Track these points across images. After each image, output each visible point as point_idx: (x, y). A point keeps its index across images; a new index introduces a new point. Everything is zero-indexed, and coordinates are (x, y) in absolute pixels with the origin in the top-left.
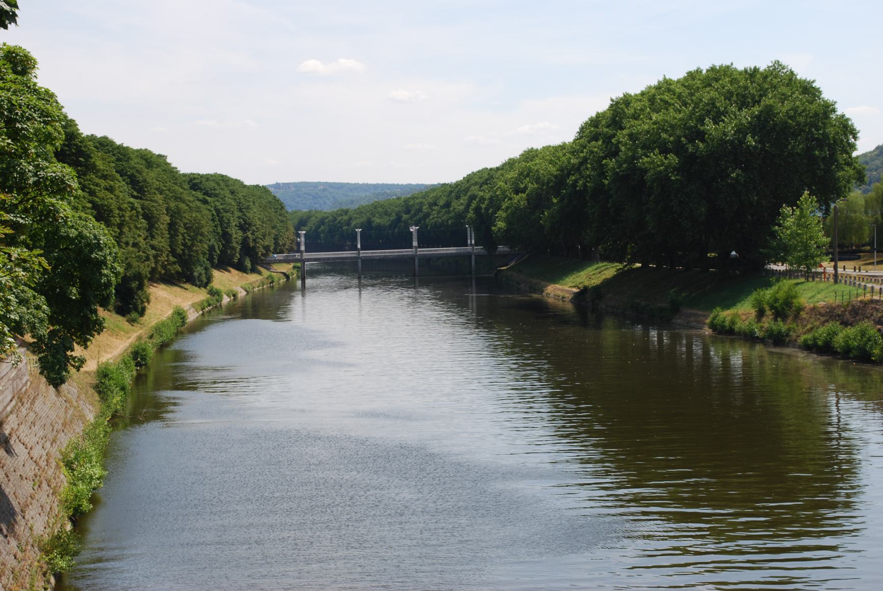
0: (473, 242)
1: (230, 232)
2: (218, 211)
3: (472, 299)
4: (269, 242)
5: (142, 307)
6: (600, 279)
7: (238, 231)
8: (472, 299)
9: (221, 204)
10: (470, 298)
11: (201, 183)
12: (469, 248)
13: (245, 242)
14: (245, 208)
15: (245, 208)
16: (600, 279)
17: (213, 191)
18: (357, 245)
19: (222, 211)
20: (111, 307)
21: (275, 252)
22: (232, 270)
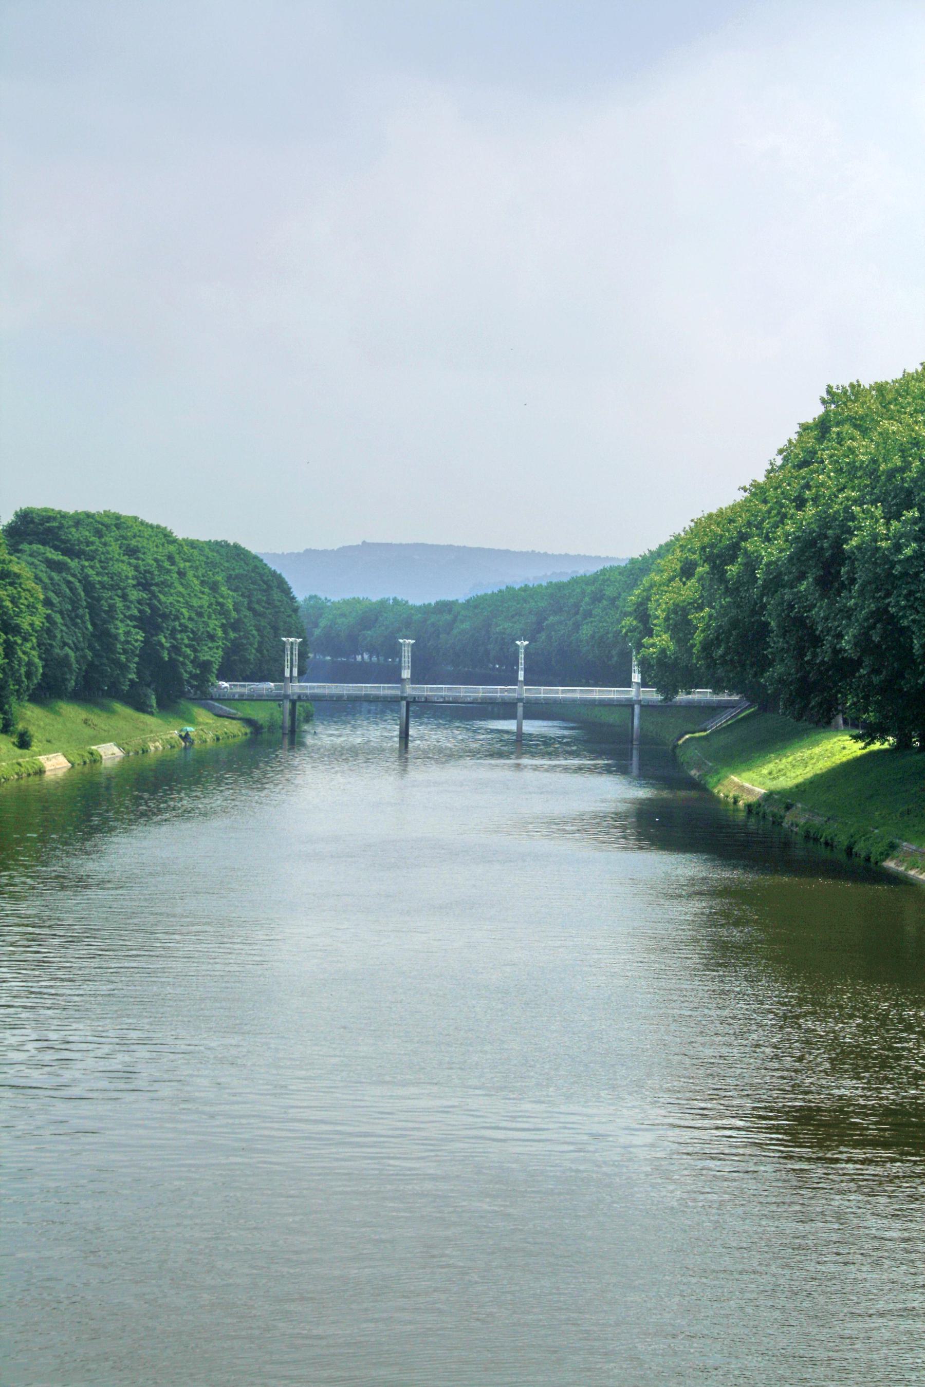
0: (295, 673)
1: (113, 631)
2: (89, 586)
3: (292, 648)
4: (213, 654)
5: (276, 690)
6: (824, 748)
7: (133, 631)
8: (292, 648)
9: (98, 574)
10: (288, 647)
11: (61, 527)
12: (632, 693)
13: (149, 653)
14: (157, 585)
15: (157, 585)
16: (824, 748)
17: (83, 547)
18: (399, 669)
19: (98, 586)
20: (155, 710)
21: (222, 676)
22: (118, 707)
